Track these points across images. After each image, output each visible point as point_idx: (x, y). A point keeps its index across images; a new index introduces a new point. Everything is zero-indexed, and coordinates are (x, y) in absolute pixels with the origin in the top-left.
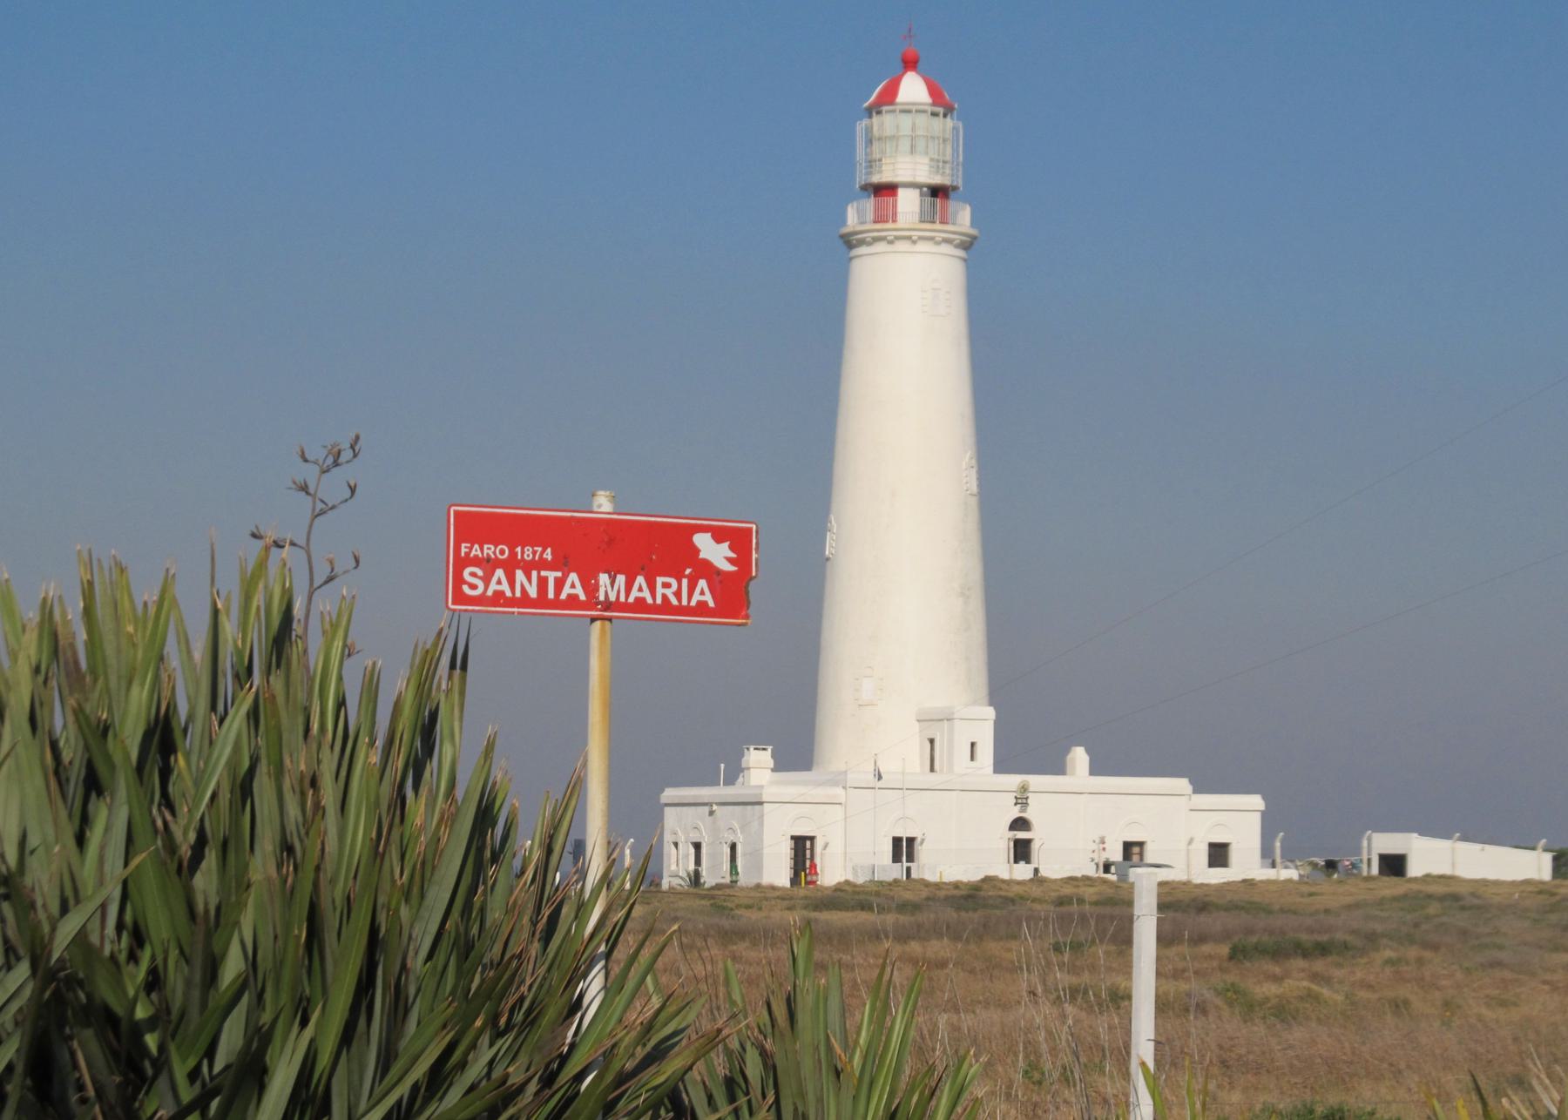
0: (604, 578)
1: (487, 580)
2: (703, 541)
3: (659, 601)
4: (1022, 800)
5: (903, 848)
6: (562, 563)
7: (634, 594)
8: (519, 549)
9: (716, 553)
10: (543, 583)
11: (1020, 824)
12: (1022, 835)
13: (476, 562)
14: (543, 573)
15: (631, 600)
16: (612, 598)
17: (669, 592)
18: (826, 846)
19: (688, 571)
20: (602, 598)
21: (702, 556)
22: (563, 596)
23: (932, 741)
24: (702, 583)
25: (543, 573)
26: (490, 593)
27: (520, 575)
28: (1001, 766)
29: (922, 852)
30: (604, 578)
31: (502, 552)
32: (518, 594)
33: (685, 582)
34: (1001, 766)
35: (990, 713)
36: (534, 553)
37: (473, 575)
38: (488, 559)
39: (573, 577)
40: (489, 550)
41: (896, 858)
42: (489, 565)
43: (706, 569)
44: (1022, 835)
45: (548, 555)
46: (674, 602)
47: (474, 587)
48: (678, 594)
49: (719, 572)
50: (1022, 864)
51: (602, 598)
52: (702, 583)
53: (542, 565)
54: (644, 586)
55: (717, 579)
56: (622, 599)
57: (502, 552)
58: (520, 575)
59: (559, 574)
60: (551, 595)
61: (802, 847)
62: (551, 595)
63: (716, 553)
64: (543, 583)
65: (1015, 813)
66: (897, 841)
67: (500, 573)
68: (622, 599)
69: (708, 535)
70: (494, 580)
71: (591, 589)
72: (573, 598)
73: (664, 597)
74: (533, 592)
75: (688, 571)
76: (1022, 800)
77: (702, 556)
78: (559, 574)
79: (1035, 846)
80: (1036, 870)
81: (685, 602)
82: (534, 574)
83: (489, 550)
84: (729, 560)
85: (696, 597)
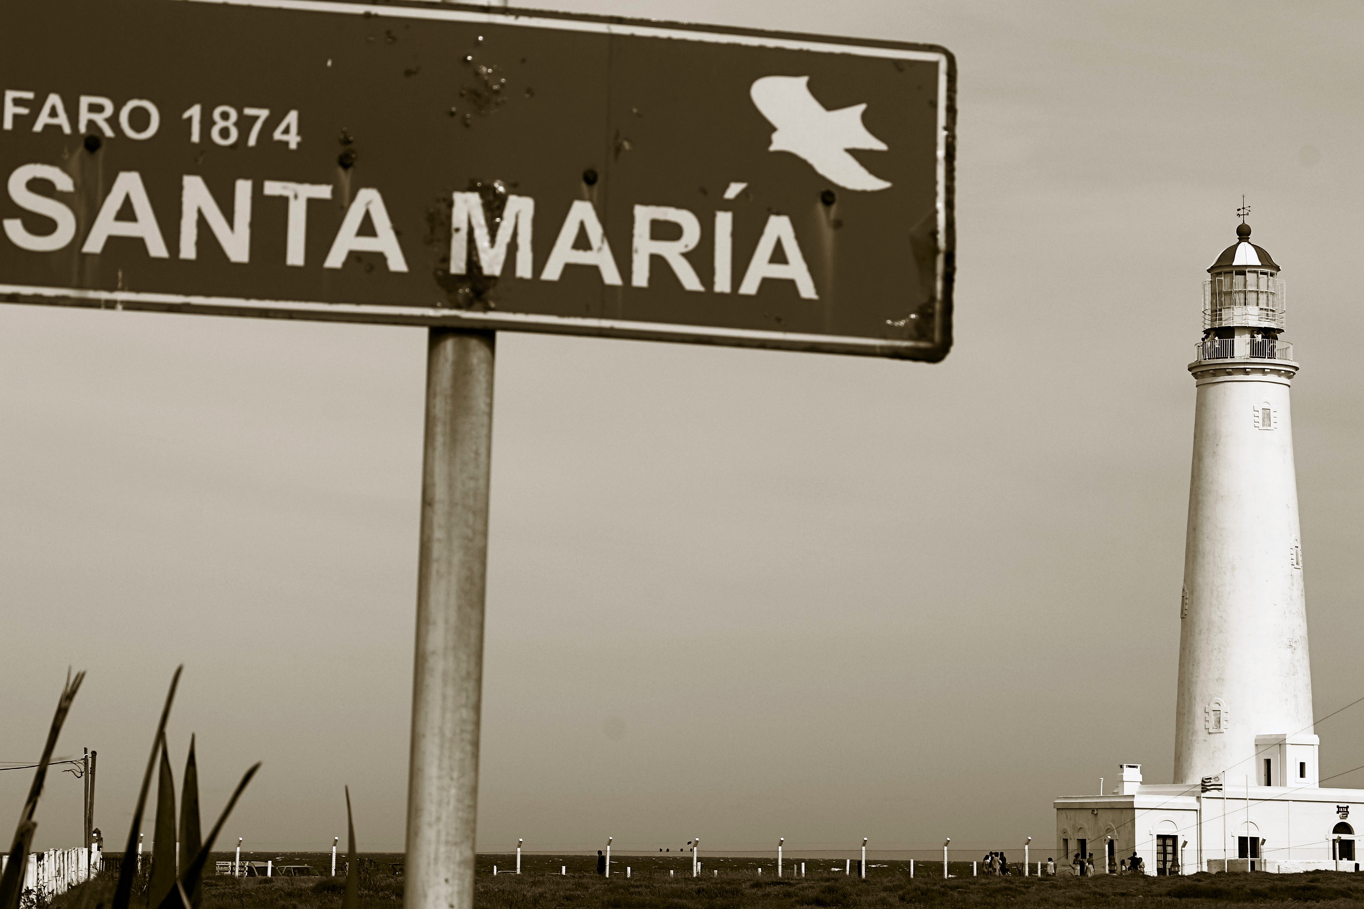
0: (467, 207)
1: (86, 207)
2: (783, 103)
3: (641, 276)
4: (1343, 811)
5: (1250, 846)
6: (339, 158)
7: (563, 254)
8: (195, 112)
9: (823, 137)
10: (269, 216)
11: (1343, 828)
12: (1345, 837)
13: (49, 147)
14: (272, 188)
15: (552, 272)
16: (492, 262)
17: (672, 252)
18: (1185, 843)
19: (734, 190)
20: (458, 265)
21: (778, 143)
22: (335, 259)
23: (1268, 762)
24: (779, 228)
25: (272, 188)
26: (94, 244)
27: (195, 193)
28: (1324, 782)
29: (1266, 852)
30: (467, 207)
31: (140, 119)
32: (188, 250)
33: (724, 222)
34: (1324, 782)
35: (1316, 739)
36: (245, 124)
37: (40, 187)
38: (93, 141)
39: (369, 200)
40: (96, 112)
41: (1242, 853)
42: (95, 158)
43: (794, 186)
44: (1345, 837)
45: (289, 131)
46: (690, 280)
47: (41, 225)
48: (701, 258)
49: (829, 193)
50: (1345, 860)
51: (458, 265)
52: (779, 228)
53: (270, 161)
54: (595, 231)
55: (823, 216)
56: (524, 269)
57: (140, 119)
58: (195, 193)
59: (324, 192)
60: (296, 255)
61: (1168, 843)
62: (296, 255)
63: (823, 137)
64: (269, 216)
65: (1337, 820)
66: (1242, 840)
67: (129, 184)
68: (524, 269)
69: (797, 86)
70: (113, 203)
71: (425, 228)
72: (366, 263)
73: (658, 264)
74: (237, 245)
75: (734, 190)
76: (1343, 811)
77: (778, 143)
78: (324, 192)
79: (1357, 846)
80: (1357, 866)
81: (722, 284)
82: (243, 189)
83: (96, 112)
84: (862, 156)
85: (760, 268)
